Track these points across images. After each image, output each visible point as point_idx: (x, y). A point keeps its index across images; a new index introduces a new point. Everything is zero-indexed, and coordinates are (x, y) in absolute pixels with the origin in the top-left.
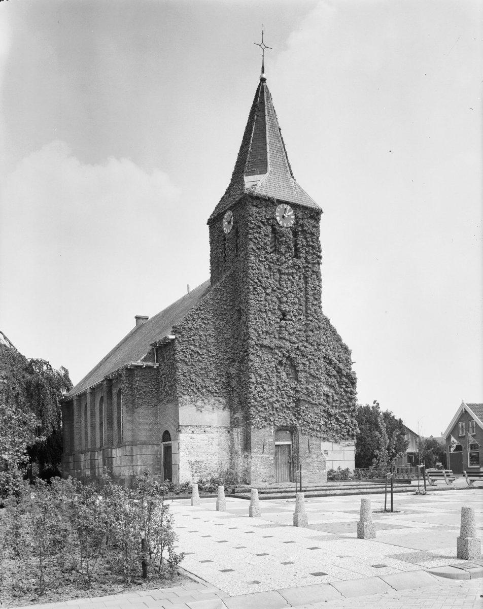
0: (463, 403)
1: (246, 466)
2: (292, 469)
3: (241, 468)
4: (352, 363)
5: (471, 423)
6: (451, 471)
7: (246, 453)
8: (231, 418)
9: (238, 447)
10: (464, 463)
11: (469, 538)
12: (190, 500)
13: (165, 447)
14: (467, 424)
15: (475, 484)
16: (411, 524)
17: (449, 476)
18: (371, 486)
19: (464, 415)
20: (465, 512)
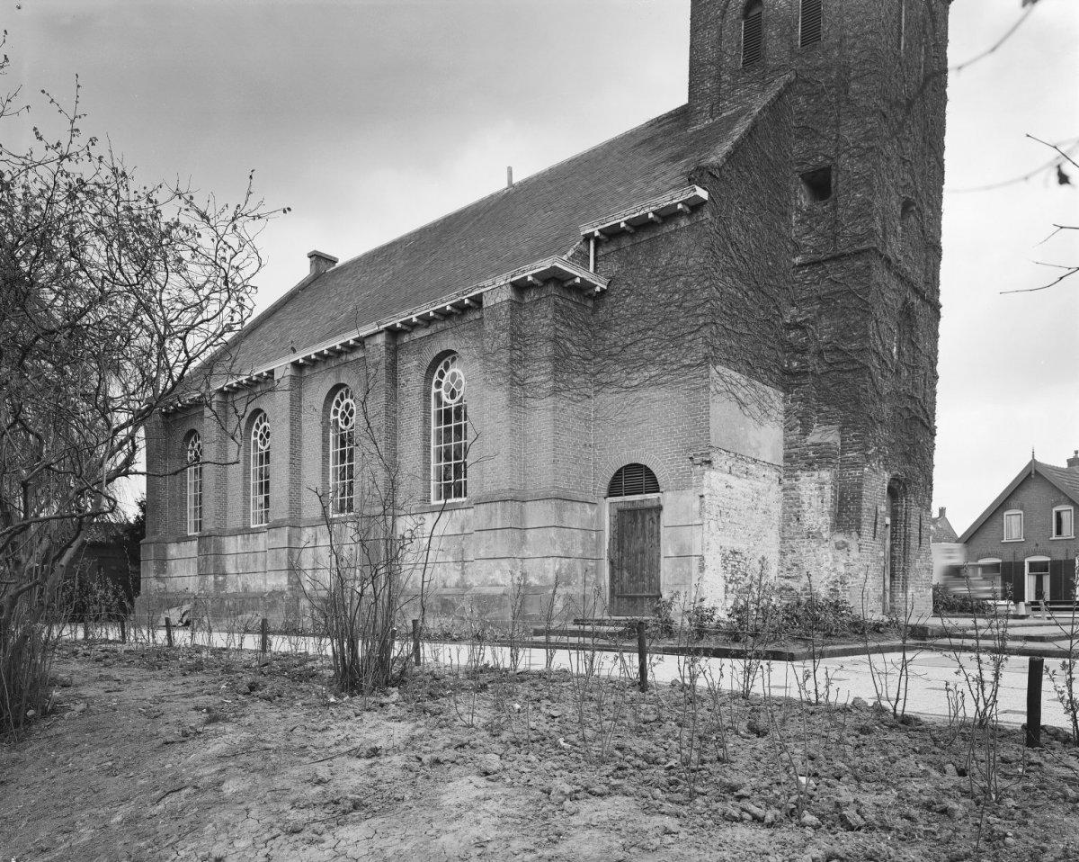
1: (842, 569)
2: (888, 583)
3: (826, 574)
7: (840, 538)
8: (789, 444)
9: (817, 514)
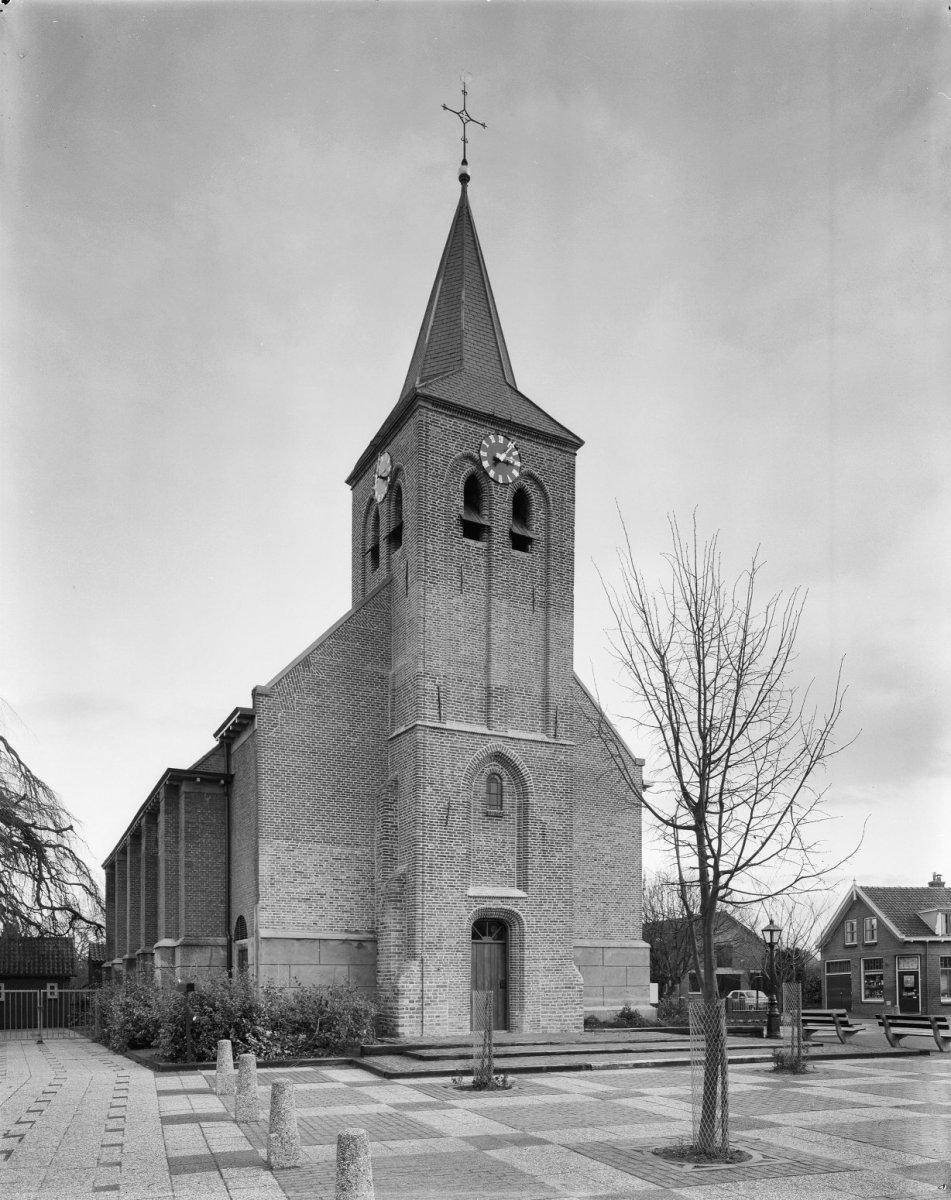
10: (854, 990)
14: (861, 924)
19: (855, 906)
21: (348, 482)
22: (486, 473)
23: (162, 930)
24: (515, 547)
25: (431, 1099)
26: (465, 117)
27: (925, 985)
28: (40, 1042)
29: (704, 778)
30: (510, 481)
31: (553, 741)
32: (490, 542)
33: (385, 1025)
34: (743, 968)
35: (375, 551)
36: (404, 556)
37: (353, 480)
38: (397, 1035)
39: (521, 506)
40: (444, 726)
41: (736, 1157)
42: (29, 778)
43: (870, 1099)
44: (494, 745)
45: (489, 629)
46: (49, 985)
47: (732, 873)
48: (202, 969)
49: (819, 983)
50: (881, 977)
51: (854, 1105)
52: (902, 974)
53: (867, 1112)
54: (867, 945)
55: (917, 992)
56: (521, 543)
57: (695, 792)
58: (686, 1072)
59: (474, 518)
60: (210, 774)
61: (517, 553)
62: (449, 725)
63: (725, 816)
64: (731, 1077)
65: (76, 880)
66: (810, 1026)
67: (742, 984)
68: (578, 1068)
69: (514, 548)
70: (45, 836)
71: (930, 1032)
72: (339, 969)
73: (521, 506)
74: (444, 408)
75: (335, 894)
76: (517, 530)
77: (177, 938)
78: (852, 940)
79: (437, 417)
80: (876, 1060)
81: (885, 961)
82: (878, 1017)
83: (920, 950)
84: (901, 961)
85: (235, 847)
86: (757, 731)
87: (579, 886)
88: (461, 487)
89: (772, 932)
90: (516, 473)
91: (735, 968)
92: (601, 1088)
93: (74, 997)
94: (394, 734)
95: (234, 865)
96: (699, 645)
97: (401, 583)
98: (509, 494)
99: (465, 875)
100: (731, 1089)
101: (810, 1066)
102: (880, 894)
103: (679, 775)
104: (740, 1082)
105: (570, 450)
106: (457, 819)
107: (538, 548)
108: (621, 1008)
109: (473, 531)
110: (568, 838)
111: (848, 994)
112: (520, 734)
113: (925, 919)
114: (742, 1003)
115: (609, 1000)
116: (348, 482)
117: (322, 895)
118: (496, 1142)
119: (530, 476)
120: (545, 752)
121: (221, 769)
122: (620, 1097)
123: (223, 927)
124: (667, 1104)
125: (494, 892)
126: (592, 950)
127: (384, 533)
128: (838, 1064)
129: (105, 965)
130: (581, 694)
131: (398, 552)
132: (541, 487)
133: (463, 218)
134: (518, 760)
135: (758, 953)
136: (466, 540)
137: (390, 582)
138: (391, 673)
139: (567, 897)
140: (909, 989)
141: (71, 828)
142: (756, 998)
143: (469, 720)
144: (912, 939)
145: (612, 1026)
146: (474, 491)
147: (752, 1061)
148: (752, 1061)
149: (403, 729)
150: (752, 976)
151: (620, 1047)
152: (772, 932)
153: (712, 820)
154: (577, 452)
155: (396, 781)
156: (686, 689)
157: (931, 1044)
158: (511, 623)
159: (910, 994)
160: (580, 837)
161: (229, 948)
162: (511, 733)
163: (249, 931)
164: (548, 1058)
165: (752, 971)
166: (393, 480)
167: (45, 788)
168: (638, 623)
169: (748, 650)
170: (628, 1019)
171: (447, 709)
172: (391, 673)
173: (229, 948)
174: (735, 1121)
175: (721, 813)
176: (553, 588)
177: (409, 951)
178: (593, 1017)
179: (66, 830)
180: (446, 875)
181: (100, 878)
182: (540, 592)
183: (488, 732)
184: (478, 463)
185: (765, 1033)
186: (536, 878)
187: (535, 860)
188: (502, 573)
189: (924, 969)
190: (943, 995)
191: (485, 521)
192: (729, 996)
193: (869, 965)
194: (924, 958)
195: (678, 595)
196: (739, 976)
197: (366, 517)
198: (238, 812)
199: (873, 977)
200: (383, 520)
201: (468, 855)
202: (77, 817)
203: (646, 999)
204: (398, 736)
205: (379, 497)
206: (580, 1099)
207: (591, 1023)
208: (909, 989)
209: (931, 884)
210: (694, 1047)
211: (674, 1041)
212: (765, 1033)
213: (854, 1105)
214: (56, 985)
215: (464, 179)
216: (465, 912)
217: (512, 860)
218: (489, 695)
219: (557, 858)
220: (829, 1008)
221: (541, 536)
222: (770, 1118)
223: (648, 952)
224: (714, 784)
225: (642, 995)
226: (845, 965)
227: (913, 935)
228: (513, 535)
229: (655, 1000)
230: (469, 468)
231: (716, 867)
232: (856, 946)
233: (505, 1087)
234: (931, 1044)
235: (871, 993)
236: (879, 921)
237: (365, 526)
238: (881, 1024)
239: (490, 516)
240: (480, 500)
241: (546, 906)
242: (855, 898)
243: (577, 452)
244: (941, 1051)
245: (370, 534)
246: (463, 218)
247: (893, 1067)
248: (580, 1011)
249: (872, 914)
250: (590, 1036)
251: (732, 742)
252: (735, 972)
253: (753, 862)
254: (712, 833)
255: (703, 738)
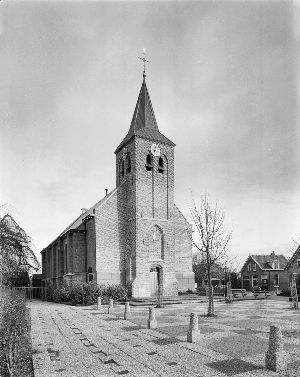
0: (250, 255)
4: (193, 232)
5: (254, 265)
6: (245, 289)
10: (250, 285)
11: (277, 353)
12: (108, 305)
13: (90, 276)
14: (252, 266)
15: (258, 297)
16: (221, 327)
17: (244, 292)
18: (201, 298)
19: (250, 261)
20: (94, 214)
21: (115, 153)
22: (152, 154)
23: (68, 271)
24: (159, 172)
25: (146, 312)
26: (144, 60)
27: (269, 282)
28: (31, 301)
29: (208, 242)
30: (158, 156)
31: (170, 221)
32: (153, 171)
33: (130, 294)
34: (219, 278)
35: (123, 173)
36: (131, 174)
37: (117, 152)
38: (132, 297)
39: (161, 161)
40: (142, 218)
41: (216, 316)
42: (18, 228)
43: (245, 307)
44: (155, 223)
45: (153, 194)
46: (22, 286)
47: (213, 260)
48: (79, 282)
49: (241, 282)
50: (258, 280)
51: (241, 308)
52: (263, 279)
53: (243, 309)
54: (254, 271)
55: (267, 285)
56: (161, 171)
57: (206, 245)
58: (206, 304)
59: (149, 165)
60: (81, 230)
61: (160, 174)
62: (144, 218)
63: (212, 249)
64: (214, 304)
65: (30, 256)
66: (236, 293)
67: (219, 283)
68: (179, 303)
69: (159, 172)
70: (23, 244)
71: (264, 294)
72: (117, 280)
73: (161, 161)
74: (141, 138)
75: (115, 261)
76: (160, 168)
77: (72, 273)
78: (255, 270)
79: (140, 140)
80: (250, 301)
81: (259, 276)
82: (252, 290)
83: (268, 273)
84: (263, 276)
85: (88, 249)
86: (218, 233)
87: (176, 258)
88: (146, 158)
89: (226, 269)
90: (159, 154)
91: (218, 279)
92: (185, 307)
93: (42, 289)
94: (129, 220)
95: (87, 254)
96: (207, 215)
97: (130, 181)
98: (158, 159)
99: (148, 256)
100: (214, 306)
101: (234, 302)
102: (257, 257)
103: (203, 241)
104: (216, 305)
105: (173, 147)
106: (146, 241)
107: (165, 172)
108: (187, 289)
109: (149, 169)
110: (174, 246)
111: (249, 285)
112: (161, 220)
113: (269, 264)
114: (219, 288)
115: (184, 287)
116: (115, 153)
117: (112, 262)
118: (168, 315)
119: (163, 154)
120: (168, 224)
121: (83, 228)
122: (190, 308)
123: (85, 270)
124: (202, 308)
125: (156, 260)
126: (180, 275)
127: (125, 168)
128: (241, 302)
129: (42, 280)
130: (176, 208)
131: (130, 174)
132: (166, 157)
133: (144, 86)
134: (161, 227)
135: (223, 274)
136: (147, 171)
137: (127, 181)
138: (128, 204)
139: (174, 261)
140: (265, 284)
141: (30, 241)
142: (222, 287)
143: (148, 216)
144: (266, 270)
145: (185, 294)
146: (149, 158)
147: (220, 301)
148: (220, 301)
149: (132, 219)
150: (222, 281)
151: (188, 299)
152: (226, 269)
153: (209, 250)
154: (174, 147)
155: (130, 232)
156: (204, 225)
157: (264, 297)
158: (159, 192)
159: (265, 285)
160: (176, 245)
161: (87, 275)
162: (159, 220)
163: (93, 270)
164: (171, 301)
165: (222, 279)
166: (128, 155)
167: (23, 230)
168: (194, 211)
169: (216, 217)
170: (189, 292)
171: (143, 214)
172: (128, 204)
173: (87, 275)
174: (215, 311)
175: (211, 248)
176: (169, 183)
177: (134, 276)
178: (180, 292)
179: (29, 242)
180: (143, 256)
181: (39, 258)
182: (166, 184)
183: (153, 220)
184: (150, 152)
185: (224, 295)
186: (166, 256)
187: (165, 252)
188: (156, 179)
189: (269, 278)
190: (275, 285)
191: (151, 166)
192: (216, 286)
193: (254, 277)
194: (269, 275)
195: (203, 206)
196: (218, 281)
197: (120, 163)
198: (89, 240)
199: (255, 280)
200: (125, 164)
201: (149, 251)
202: (32, 238)
203: (194, 287)
204: (130, 221)
205: (124, 159)
206: (181, 309)
207: (180, 293)
208: (265, 284)
209: (271, 254)
210: (206, 299)
211: (202, 297)
212: (224, 295)
213: (241, 308)
214: (24, 286)
215: (144, 76)
216: (148, 265)
217: (160, 252)
218: (153, 210)
219: (171, 251)
220: (243, 289)
221: (166, 169)
222: (223, 311)
223: (194, 275)
224: (210, 243)
225: (193, 286)
226: (248, 277)
227: (266, 268)
228: (159, 169)
229: (196, 287)
230: (148, 153)
231: (210, 259)
232: (250, 272)
233: (163, 307)
234: (264, 297)
235: (255, 284)
236: (257, 265)
237: (120, 165)
238: (253, 292)
239: (153, 165)
240: (151, 160)
241: (168, 264)
242: (250, 258)
243: (174, 147)
244: (267, 298)
245: (121, 167)
246: (144, 86)
247: (253, 302)
248: (177, 290)
249: (255, 263)
250: (180, 296)
251: (213, 235)
252: (218, 280)
253: (218, 258)
254: (210, 253)
255: (208, 234)
